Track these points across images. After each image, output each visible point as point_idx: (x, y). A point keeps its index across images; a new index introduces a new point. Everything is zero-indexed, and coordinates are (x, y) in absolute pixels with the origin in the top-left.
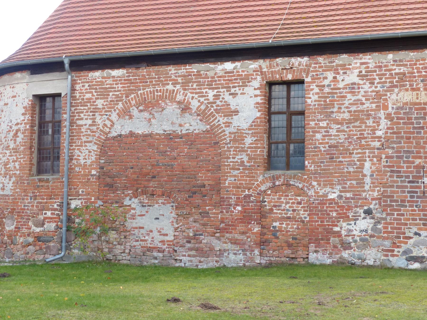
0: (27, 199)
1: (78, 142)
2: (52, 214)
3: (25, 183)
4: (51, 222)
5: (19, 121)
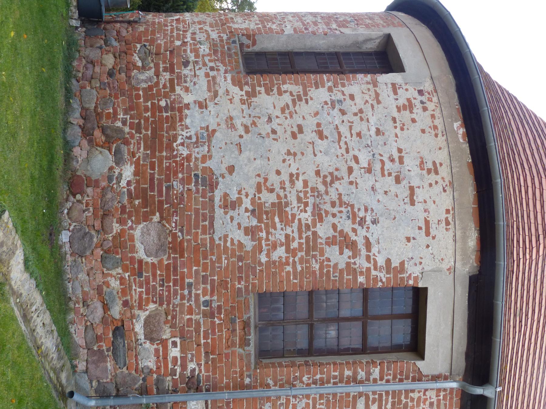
0: (205, 294)
1: (322, 404)
2: (175, 359)
3: (239, 283)
4: (158, 358)
5: (374, 250)
